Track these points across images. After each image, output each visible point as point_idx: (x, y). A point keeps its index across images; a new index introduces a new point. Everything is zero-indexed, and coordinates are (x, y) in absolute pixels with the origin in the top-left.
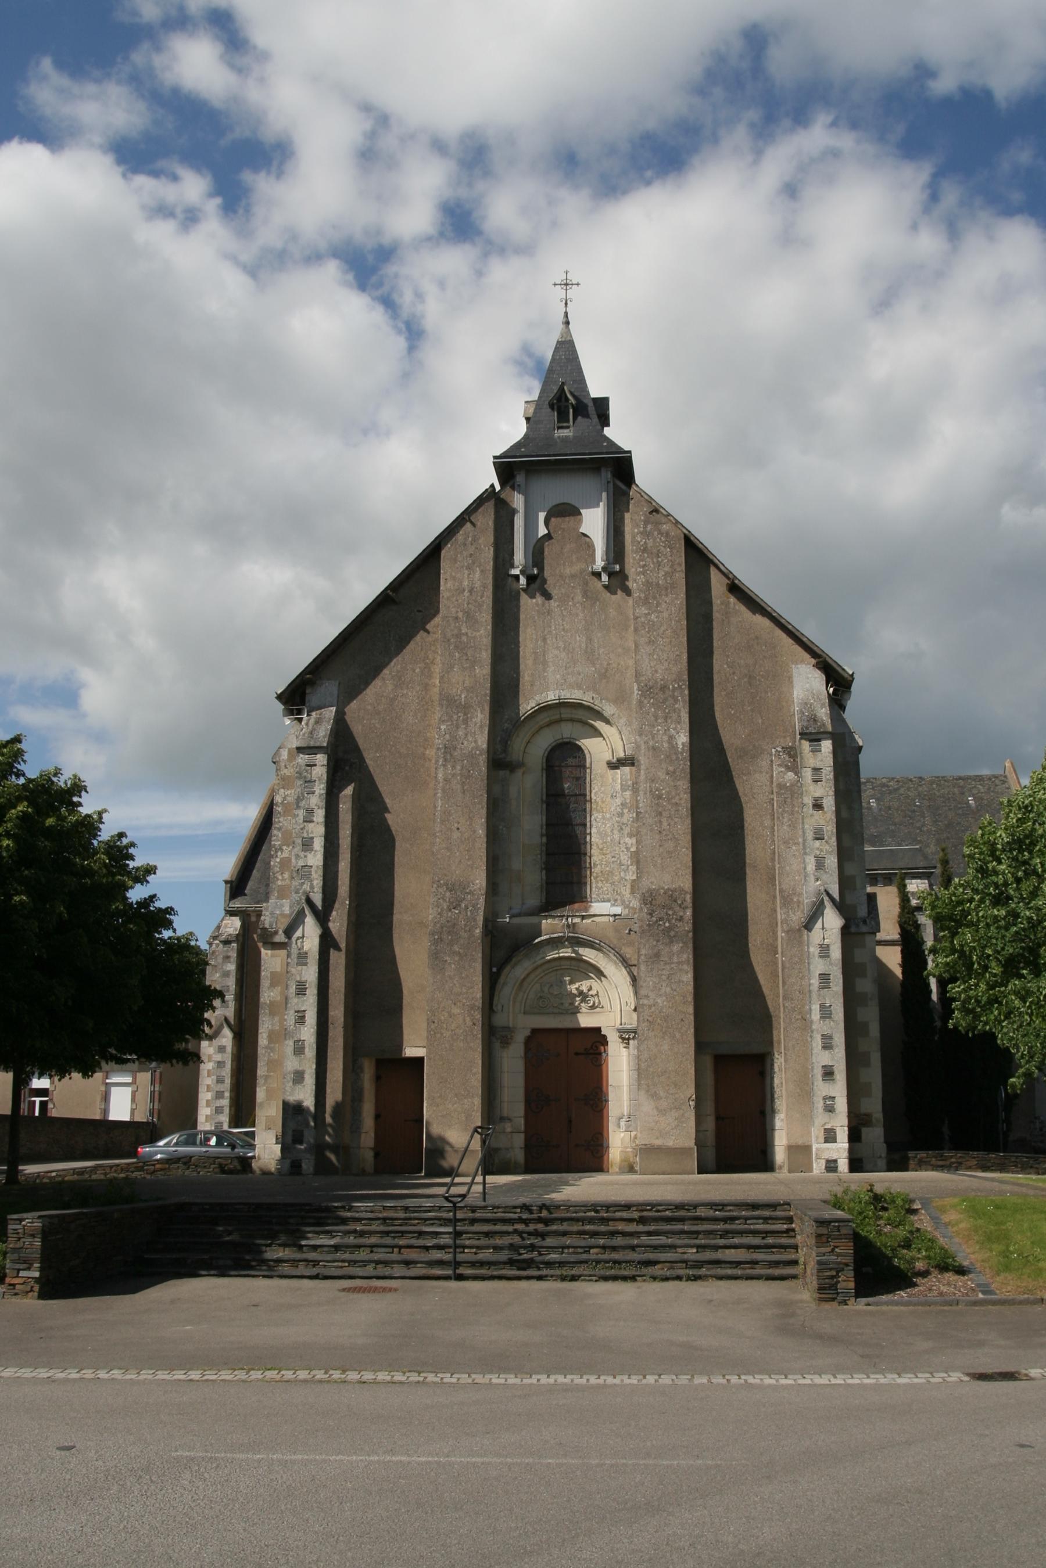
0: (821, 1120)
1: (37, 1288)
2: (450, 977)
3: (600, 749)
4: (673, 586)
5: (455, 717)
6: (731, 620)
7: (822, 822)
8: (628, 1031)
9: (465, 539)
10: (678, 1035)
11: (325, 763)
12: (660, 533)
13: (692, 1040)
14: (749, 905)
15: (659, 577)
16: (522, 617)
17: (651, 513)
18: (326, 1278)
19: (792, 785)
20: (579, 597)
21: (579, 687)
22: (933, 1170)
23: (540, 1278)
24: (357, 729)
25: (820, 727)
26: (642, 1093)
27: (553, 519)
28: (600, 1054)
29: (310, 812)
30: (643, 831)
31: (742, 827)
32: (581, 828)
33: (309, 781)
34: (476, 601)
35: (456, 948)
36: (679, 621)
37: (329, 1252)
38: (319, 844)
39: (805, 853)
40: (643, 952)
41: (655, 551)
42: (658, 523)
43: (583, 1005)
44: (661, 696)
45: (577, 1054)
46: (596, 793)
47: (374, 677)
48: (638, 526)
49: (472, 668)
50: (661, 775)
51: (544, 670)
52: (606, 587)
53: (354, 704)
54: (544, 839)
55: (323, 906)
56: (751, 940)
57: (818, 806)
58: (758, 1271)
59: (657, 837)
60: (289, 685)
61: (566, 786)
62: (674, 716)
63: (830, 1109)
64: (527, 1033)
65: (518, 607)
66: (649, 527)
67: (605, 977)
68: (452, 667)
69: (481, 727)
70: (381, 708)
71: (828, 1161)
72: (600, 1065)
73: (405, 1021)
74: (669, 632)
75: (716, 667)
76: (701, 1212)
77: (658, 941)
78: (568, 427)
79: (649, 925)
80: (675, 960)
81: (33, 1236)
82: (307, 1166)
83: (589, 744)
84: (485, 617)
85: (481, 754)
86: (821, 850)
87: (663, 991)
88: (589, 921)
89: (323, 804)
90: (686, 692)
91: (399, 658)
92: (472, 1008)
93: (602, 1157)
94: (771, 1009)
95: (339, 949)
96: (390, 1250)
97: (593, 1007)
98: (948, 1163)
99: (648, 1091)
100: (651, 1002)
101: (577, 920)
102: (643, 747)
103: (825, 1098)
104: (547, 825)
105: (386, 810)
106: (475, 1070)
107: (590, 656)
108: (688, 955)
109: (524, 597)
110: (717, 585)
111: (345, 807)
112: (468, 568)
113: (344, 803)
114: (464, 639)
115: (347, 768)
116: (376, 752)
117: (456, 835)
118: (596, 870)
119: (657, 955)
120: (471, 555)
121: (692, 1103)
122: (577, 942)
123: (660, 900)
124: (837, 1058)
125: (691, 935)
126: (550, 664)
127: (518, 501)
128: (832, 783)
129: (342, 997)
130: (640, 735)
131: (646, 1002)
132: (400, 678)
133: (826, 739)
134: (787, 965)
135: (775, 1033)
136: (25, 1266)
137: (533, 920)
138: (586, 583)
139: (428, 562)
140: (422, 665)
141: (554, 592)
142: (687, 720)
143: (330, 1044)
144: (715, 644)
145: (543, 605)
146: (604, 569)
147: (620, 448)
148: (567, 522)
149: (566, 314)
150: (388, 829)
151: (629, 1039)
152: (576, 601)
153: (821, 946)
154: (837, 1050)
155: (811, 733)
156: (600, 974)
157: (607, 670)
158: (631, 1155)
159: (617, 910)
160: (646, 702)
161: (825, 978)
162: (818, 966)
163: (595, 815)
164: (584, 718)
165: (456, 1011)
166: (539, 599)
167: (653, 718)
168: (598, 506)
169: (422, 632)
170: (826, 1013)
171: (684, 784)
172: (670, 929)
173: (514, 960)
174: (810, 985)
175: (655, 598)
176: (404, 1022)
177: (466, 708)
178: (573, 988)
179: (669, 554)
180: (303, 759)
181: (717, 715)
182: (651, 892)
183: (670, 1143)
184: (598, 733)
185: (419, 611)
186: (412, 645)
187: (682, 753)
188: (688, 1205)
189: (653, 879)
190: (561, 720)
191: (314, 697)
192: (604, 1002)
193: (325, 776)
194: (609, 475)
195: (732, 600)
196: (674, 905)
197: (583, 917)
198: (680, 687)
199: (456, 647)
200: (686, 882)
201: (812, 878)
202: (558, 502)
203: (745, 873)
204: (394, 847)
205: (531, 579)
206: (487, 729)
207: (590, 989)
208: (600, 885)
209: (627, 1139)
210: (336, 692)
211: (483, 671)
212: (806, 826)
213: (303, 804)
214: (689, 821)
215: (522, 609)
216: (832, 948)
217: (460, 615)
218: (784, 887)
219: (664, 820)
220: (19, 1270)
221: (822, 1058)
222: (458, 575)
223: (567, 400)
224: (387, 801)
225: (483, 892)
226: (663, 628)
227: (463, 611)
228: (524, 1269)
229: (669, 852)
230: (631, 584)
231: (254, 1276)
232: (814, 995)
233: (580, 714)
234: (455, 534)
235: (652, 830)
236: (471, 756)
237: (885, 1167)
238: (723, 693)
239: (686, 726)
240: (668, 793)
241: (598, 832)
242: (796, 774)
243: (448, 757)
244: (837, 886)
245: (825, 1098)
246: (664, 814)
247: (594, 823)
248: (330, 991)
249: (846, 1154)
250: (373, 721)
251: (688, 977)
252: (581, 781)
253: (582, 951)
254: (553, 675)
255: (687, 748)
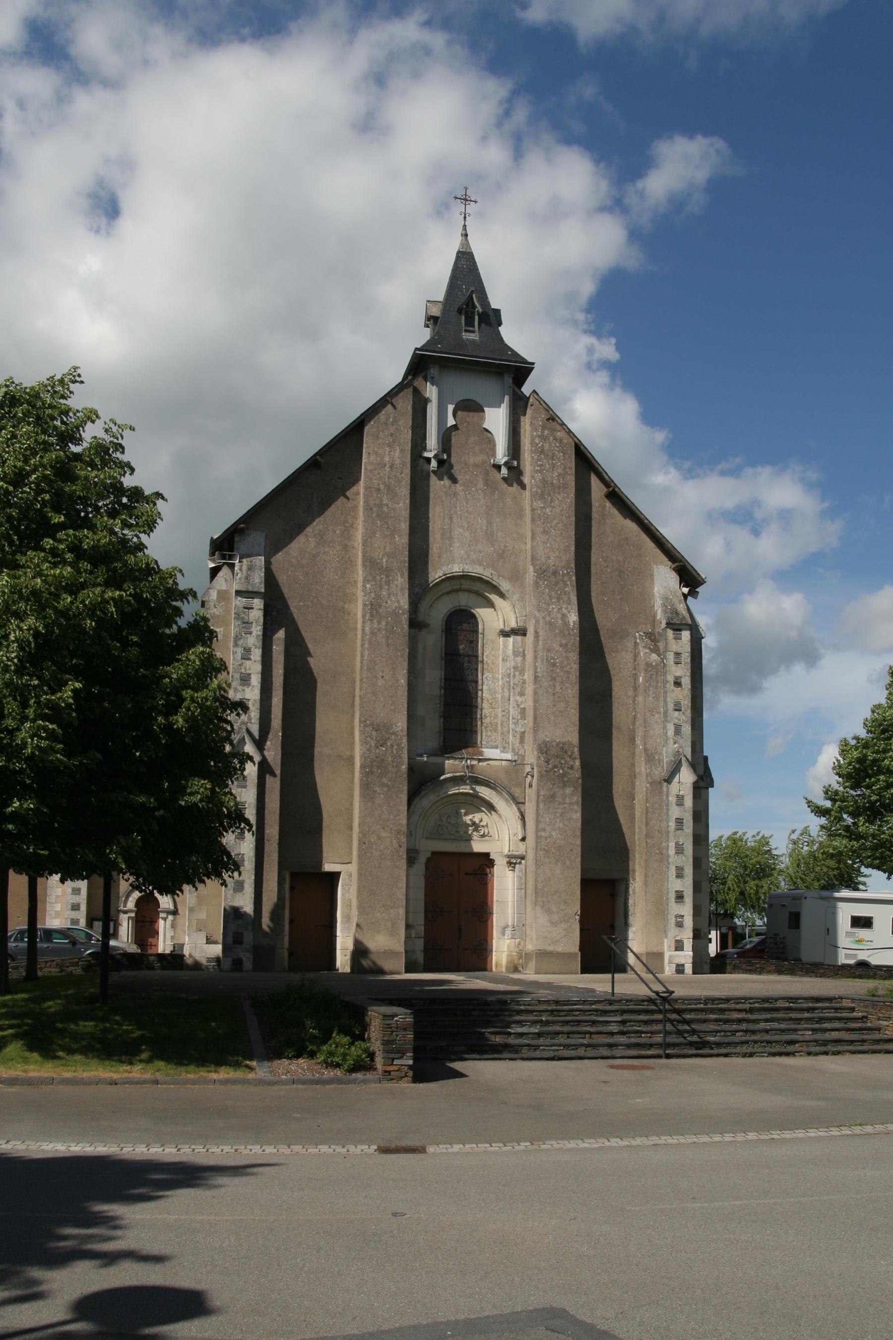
0: (673, 933)
1: (411, 1073)
2: (379, 804)
3: (493, 618)
4: (565, 486)
5: (378, 578)
6: (608, 521)
7: (680, 697)
8: (516, 857)
9: (387, 419)
10: (568, 863)
11: (262, 607)
12: (555, 439)
13: (579, 867)
14: (614, 759)
15: (554, 477)
16: (432, 495)
17: (548, 419)
18: (560, 1059)
19: (657, 665)
20: (481, 485)
21: (480, 564)
22: (743, 973)
23: (726, 1055)
24: (282, 579)
25: (682, 619)
26: (538, 908)
27: (459, 413)
28: (486, 874)
29: (247, 651)
30: (540, 692)
31: (610, 695)
32: (474, 685)
33: (247, 623)
34: (396, 477)
35: (385, 780)
36: (569, 517)
37: (533, 1039)
38: (256, 680)
39: (667, 721)
40: (542, 793)
41: (550, 454)
42: (553, 430)
43: (475, 833)
44: (553, 579)
45: (467, 874)
46: (487, 656)
47: (298, 534)
48: (536, 430)
49: (392, 536)
50: (556, 646)
51: (451, 546)
52: (504, 479)
53: (279, 556)
54: (443, 692)
55: (260, 736)
56: (614, 787)
57: (678, 684)
58: (865, 1048)
59: (551, 698)
60: (224, 532)
61: (461, 647)
62: (565, 598)
63: (680, 925)
64: (429, 855)
65: (428, 486)
66: (546, 432)
67: (495, 811)
68: (375, 533)
69: (402, 589)
70: (304, 562)
71: (678, 965)
72: (486, 884)
73: (324, 841)
74: (560, 525)
75: (593, 560)
76: (781, 1004)
77: (554, 785)
78: (473, 332)
79: (546, 771)
80: (567, 801)
81: (405, 1029)
82: (248, 964)
83: (483, 614)
84: (404, 491)
85: (403, 613)
86: (679, 720)
87: (557, 826)
88: (485, 764)
89: (260, 644)
90: (574, 578)
91: (322, 518)
92: (398, 833)
93: (486, 959)
94: (629, 844)
95: (274, 775)
96: (583, 1036)
97: (483, 836)
98: (754, 968)
99: (543, 907)
100: (547, 834)
101: (474, 762)
102: (541, 621)
103: (676, 916)
104: (445, 679)
105: (309, 654)
106: (400, 885)
107: (490, 537)
108: (577, 798)
109: (433, 478)
110: (597, 489)
111: (278, 649)
112: (389, 445)
113: (277, 645)
114: (385, 509)
115: (275, 613)
116: (300, 601)
117: (381, 682)
118: (486, 721)
119: (553, 796)
120: (392, 435)
121: (578, 918)
122: (477, 781)
123: (553, 751)
124: (686, 885)
125: (580, 781)
126: (456, 540)
127: (431, 391)
128: (689, 666)
129: (278, 817)
130: (539, 611)
131: (543, 834)
132: (322, 537)
133: (686, 630)
134: (650, 810)
135: (631, 863)
136: (399, 1055)
137: (437, 760)
138: (487, 474)
139: (354, 433)
140: (342, 528)
141: (459, 477)
142: (576, 602)
143: (266, 858)
144: (593, 540)
145: (450, 487)
146: (506, 464)
147: (523, 358)
148: (472, 417)
149: (465, 226)
150: (310, 671)
151: (515, 864)
152: (478, 487)
153: (678, 796)
154: (686, 879)
155: (675, 624)
156: (491, 807)
157: (504, 551)
158: (516, 958)
159: (509, 756)
160: (541, 583)
161: (679, 822)
162: (675, 812)
163: (486, 674)
164: (481, 591)
165: (384, 834)
166: (446, 482)
167: (548, 598)
168: (499, 406)
169: (342, 498)
170: (679, 850)
171: (574, 656)
172: (563, 775)
173: (423, 793)
174: (668, 826)
175: (549, 495)
176: (324, 841)
177: (388, 571)
178: (467, 819)
179: (562, 458)
180: (241, 601)
181: (593, 600)
182: (545, 742)
183: (560, 949)
184: (491, 605)
185: (340, 478)
186: (333, 508)
187: (573, 630)
188: (772, 999)
189: (548, 733)
190: (460, 590)
191: (242, 545)
192: (493, 831)
193: (262, 619)
194: (511, 381)
195: (608, 504)
196: (565, 756)
197: (480, 760)
198: (568, 573)
199: (378, 516)
200: (573, 737)
201: (672, 742)
202: (465, 398)
203: (611, 734)
204: (316, 687)
205: (441, 463)
206: (407, 591)
207: (481, 821)
208: (489, 733)
209: (513, 944)
210: (263, 544)
211: (402, 540)
212: (668, 699)
213: (240, 642)
214: (577, 687)
215: (431, 489)
216: (686, 798)
217: (382, 487)
218: (648, 746)
219: (557, 684)
220: (393, 1059)
221: (676, 885)
222: (380, 451)
223: (474, 307)
224: (310, 646)
225: (405, 733)
226: (555, 522)
227: (384, 483)
228: (700, 1049)
229: (560, 712)
230: (526, 480)
231: (500, 1059)
232: (671, 835)
233: (478, 586)
234: (377, 413)
235: (547, 692)
236: (395, 614)
237: (709, 971)
238: (599, 582)
239: (575, 607)
240: (561, 662)
241: (489, 689)
242: (659, 655)
243: (374, 613)
244: (690, 749)
245: (676, 916)
246: (557, 679)
247: (485, 681)
248: (266, 812)
249: (691, 960)
250: (297, 573)
251: (577, 816)
252: (473, 643)
253: (479, 789)
254: (458, 550)
255: (577, 626)
